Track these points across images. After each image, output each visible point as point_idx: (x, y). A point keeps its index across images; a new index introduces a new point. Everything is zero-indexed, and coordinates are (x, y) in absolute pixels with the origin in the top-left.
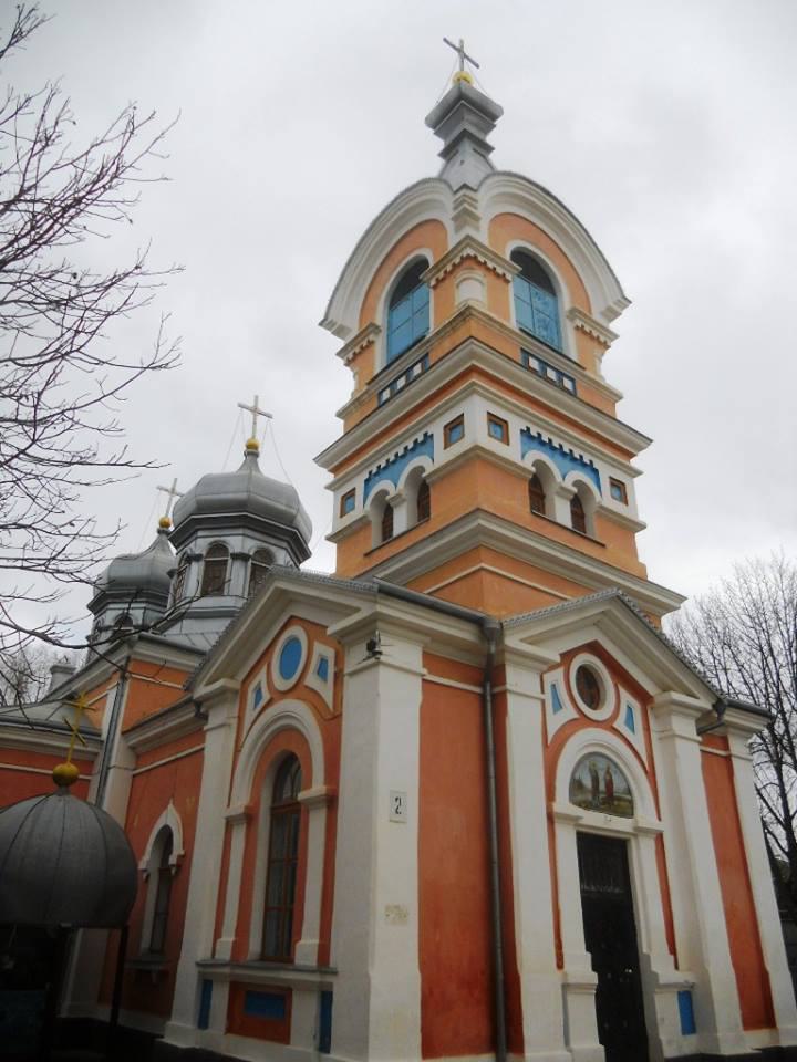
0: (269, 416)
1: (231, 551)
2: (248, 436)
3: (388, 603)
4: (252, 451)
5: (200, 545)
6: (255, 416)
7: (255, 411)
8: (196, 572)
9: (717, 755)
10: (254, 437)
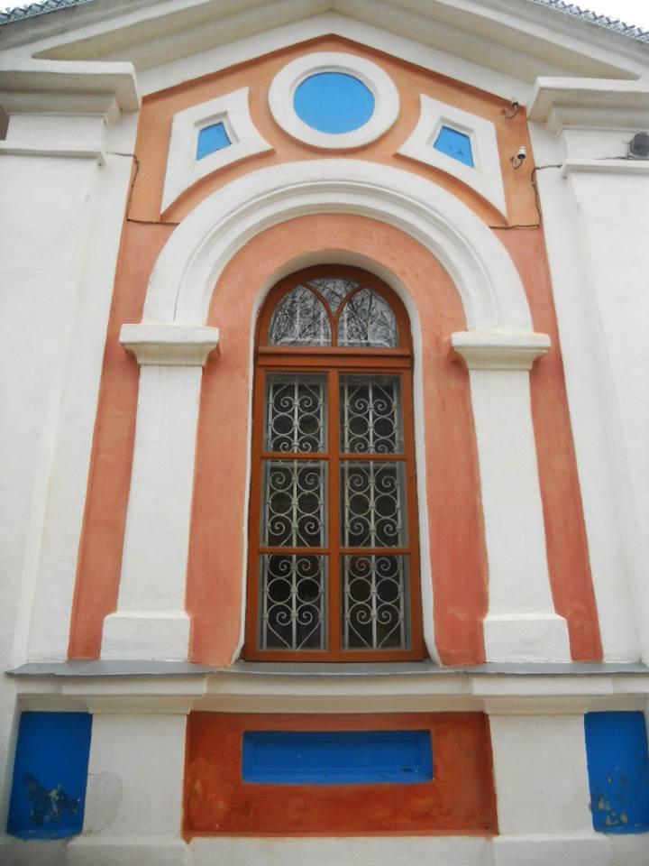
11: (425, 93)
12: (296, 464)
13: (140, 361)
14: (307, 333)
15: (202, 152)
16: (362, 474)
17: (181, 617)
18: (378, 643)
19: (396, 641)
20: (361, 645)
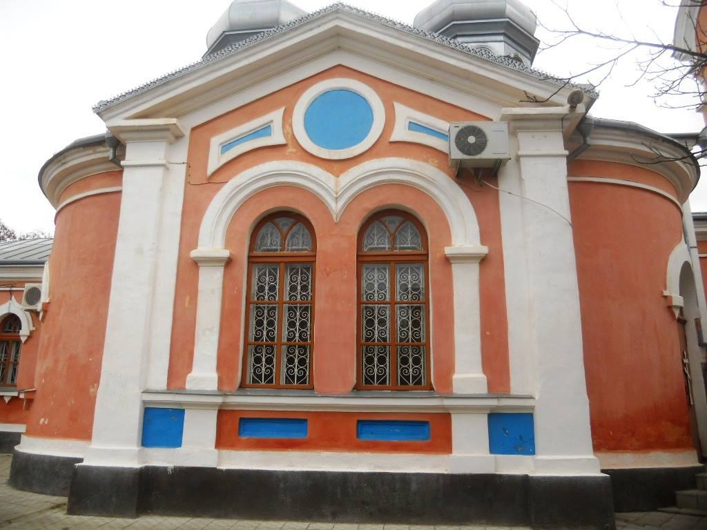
3: (68, 159)
11: (396, 101)
12: (298, 305)
13: (199, 265)
14: (379, 242)
15: (223, 152)
16: (262, 309)
17: (214, 376)
18: (412, 382)
19: (413, 381)
20: (290, 383)
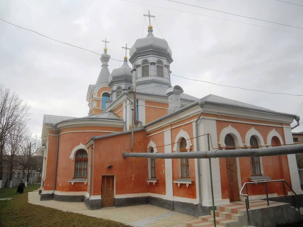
0: (154, 17)
1: (149, 62)
2: (125, 56)
4: (150, 30)
5: (139, 61)
6: (149, 17)
7: (149, 16)
8: (139, 70)
9: (279, 127)
10: (126, 56)
